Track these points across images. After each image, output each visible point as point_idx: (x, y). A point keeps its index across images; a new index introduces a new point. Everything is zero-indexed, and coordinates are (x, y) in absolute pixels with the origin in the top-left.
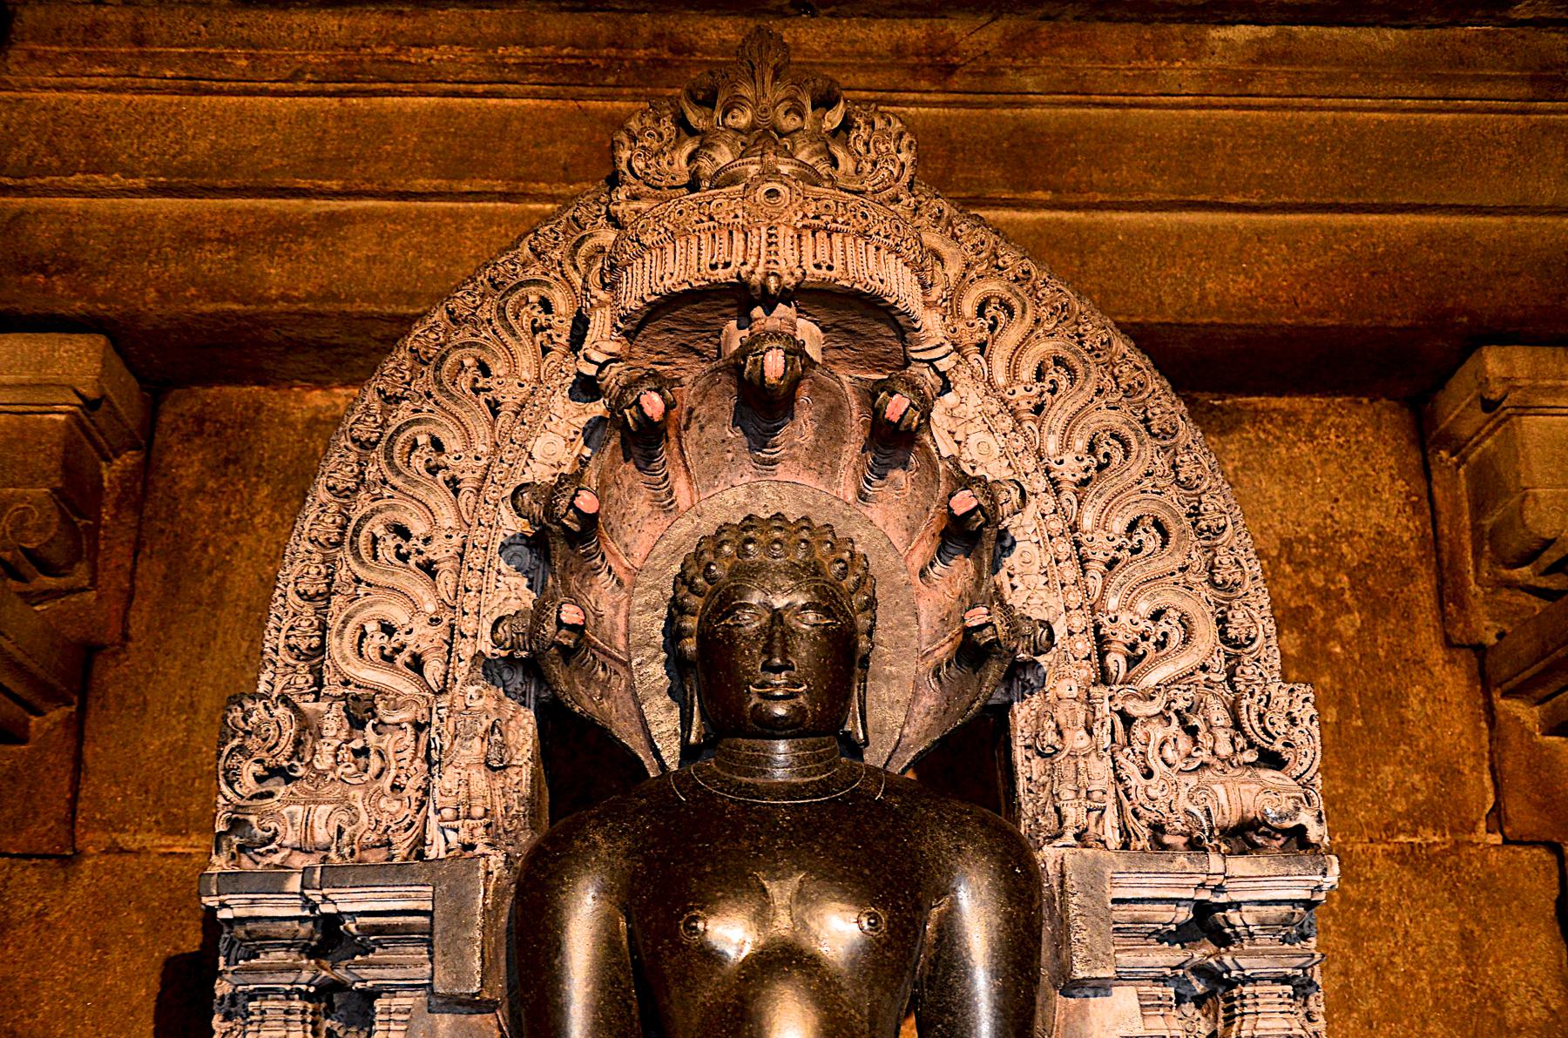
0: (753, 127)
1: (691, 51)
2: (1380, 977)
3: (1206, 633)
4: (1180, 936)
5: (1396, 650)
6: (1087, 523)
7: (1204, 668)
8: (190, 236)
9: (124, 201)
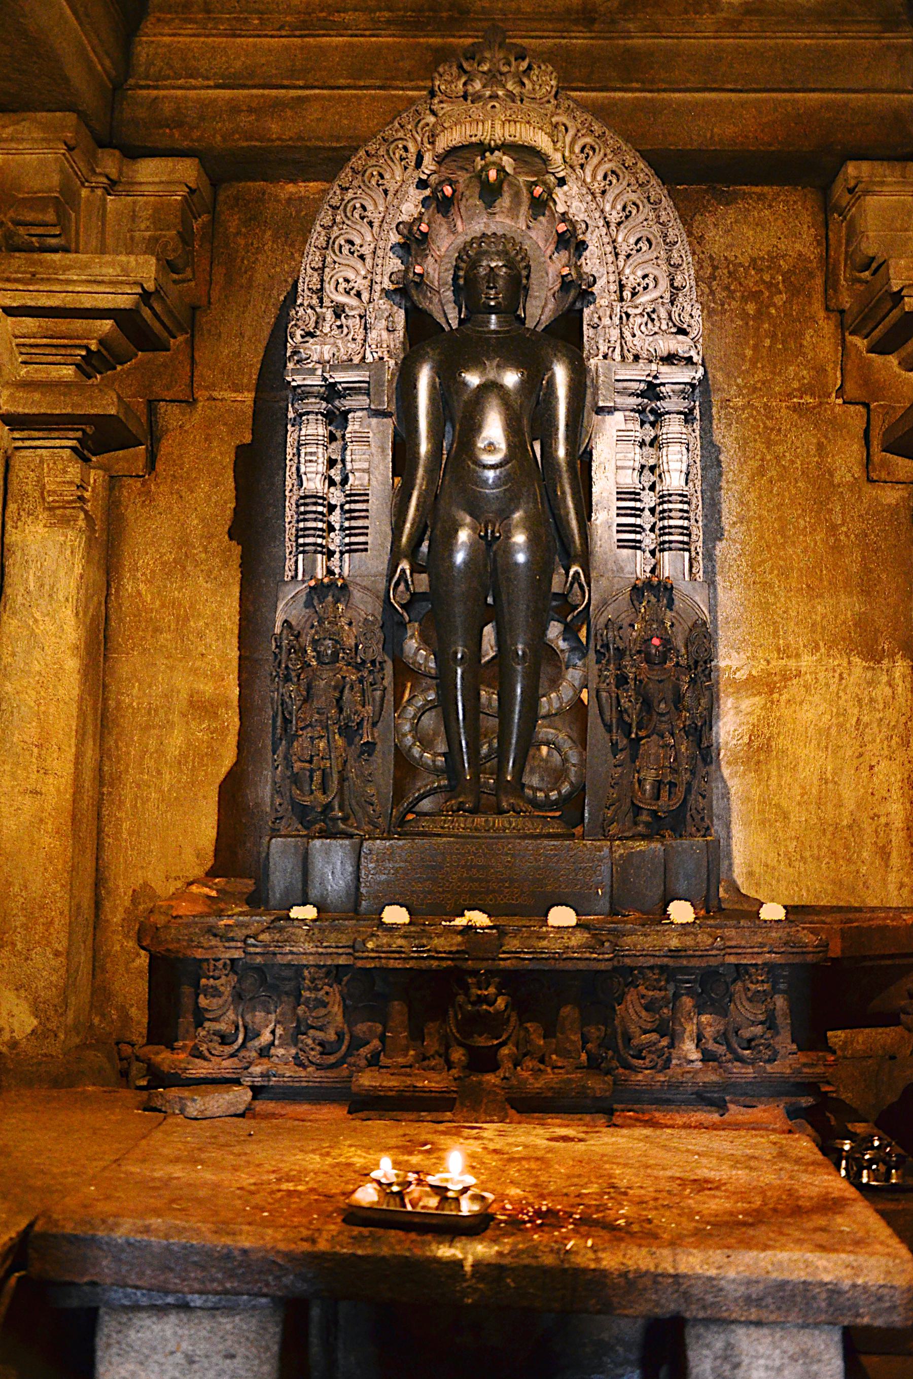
0: (490, 70)
2: (778, 462)
3: (664, 283)
4: (642, 395)
7: (662, 297)
8: (234, 109)
9: (203, 92)
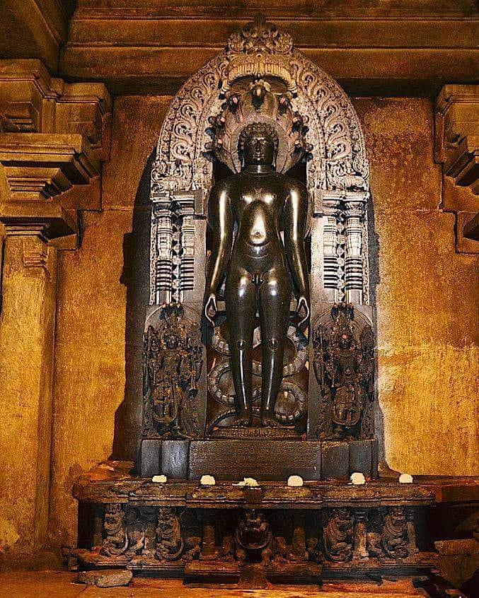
0: (257, 37)
1: (246, 7)
3: (349, 149)
5: (421, 164)
6: (326, 125)
8: (123, 57)
